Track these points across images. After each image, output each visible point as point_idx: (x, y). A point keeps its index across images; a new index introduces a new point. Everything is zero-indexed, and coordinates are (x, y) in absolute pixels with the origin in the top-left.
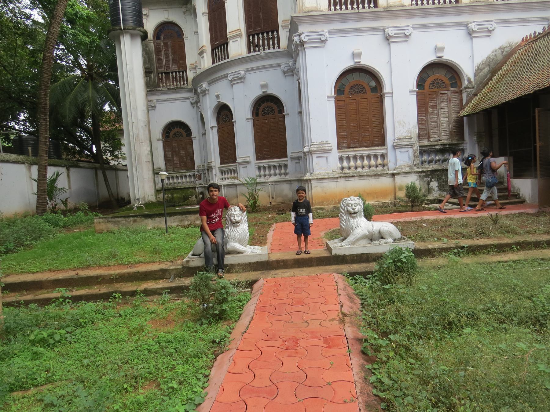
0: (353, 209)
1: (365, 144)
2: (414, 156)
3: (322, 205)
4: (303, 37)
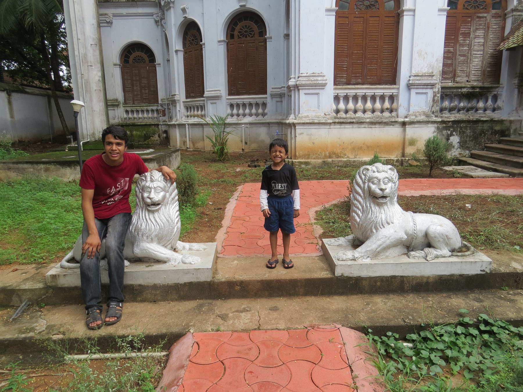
0: (381, 190)
1: (369, 80)
2: (434, 100)
3: (308, 158)
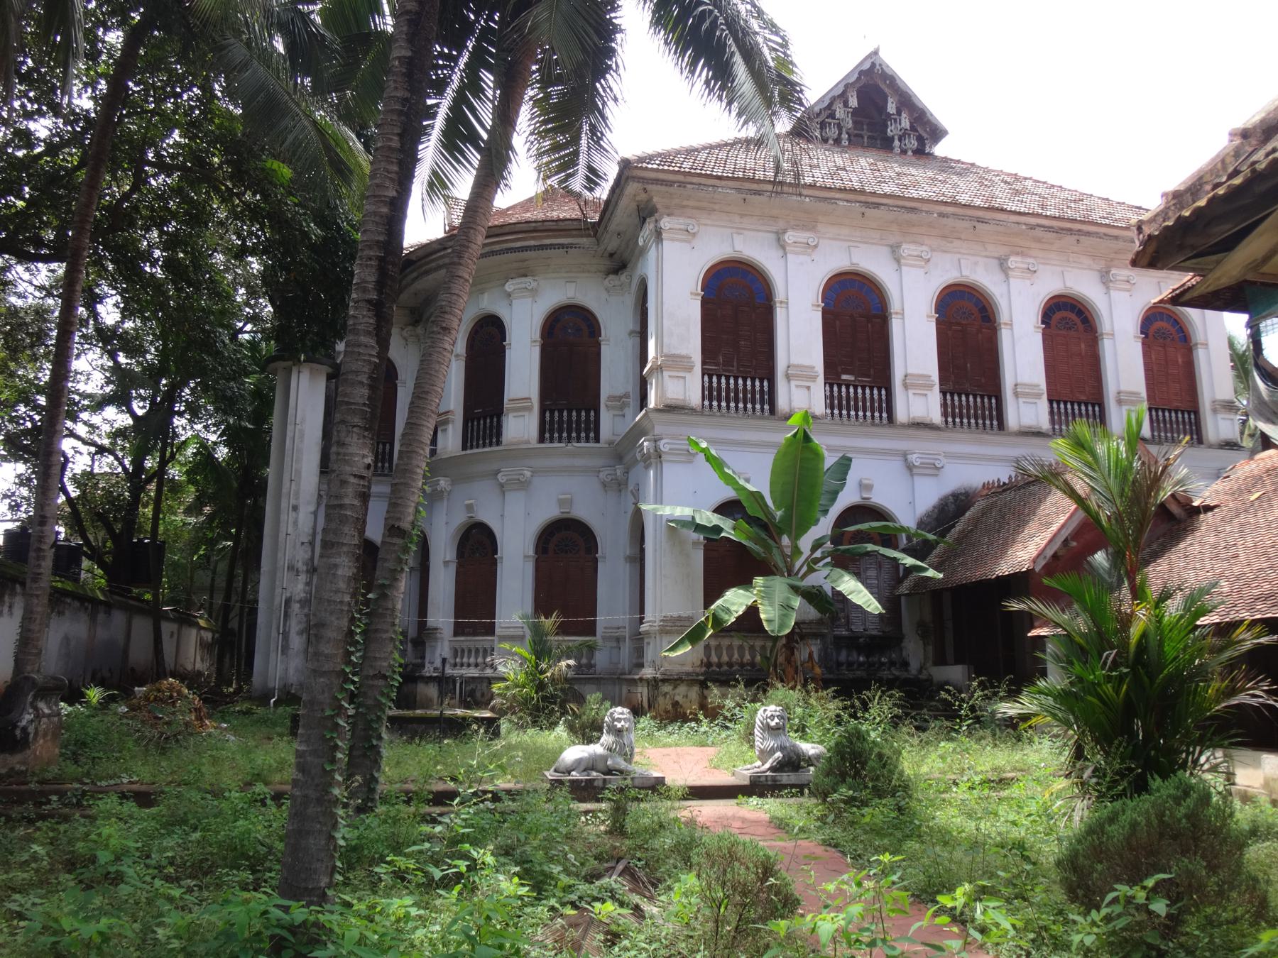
4: (661, 444)
